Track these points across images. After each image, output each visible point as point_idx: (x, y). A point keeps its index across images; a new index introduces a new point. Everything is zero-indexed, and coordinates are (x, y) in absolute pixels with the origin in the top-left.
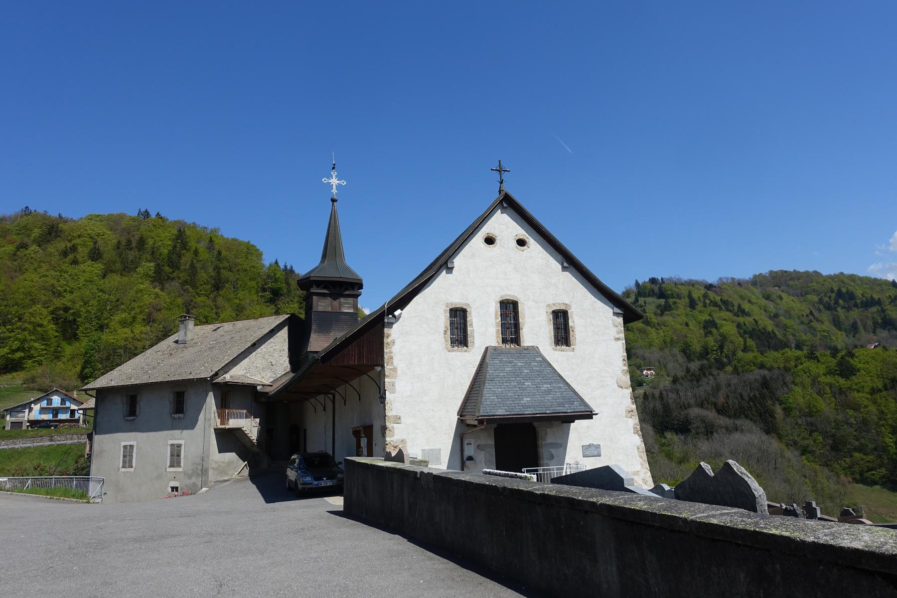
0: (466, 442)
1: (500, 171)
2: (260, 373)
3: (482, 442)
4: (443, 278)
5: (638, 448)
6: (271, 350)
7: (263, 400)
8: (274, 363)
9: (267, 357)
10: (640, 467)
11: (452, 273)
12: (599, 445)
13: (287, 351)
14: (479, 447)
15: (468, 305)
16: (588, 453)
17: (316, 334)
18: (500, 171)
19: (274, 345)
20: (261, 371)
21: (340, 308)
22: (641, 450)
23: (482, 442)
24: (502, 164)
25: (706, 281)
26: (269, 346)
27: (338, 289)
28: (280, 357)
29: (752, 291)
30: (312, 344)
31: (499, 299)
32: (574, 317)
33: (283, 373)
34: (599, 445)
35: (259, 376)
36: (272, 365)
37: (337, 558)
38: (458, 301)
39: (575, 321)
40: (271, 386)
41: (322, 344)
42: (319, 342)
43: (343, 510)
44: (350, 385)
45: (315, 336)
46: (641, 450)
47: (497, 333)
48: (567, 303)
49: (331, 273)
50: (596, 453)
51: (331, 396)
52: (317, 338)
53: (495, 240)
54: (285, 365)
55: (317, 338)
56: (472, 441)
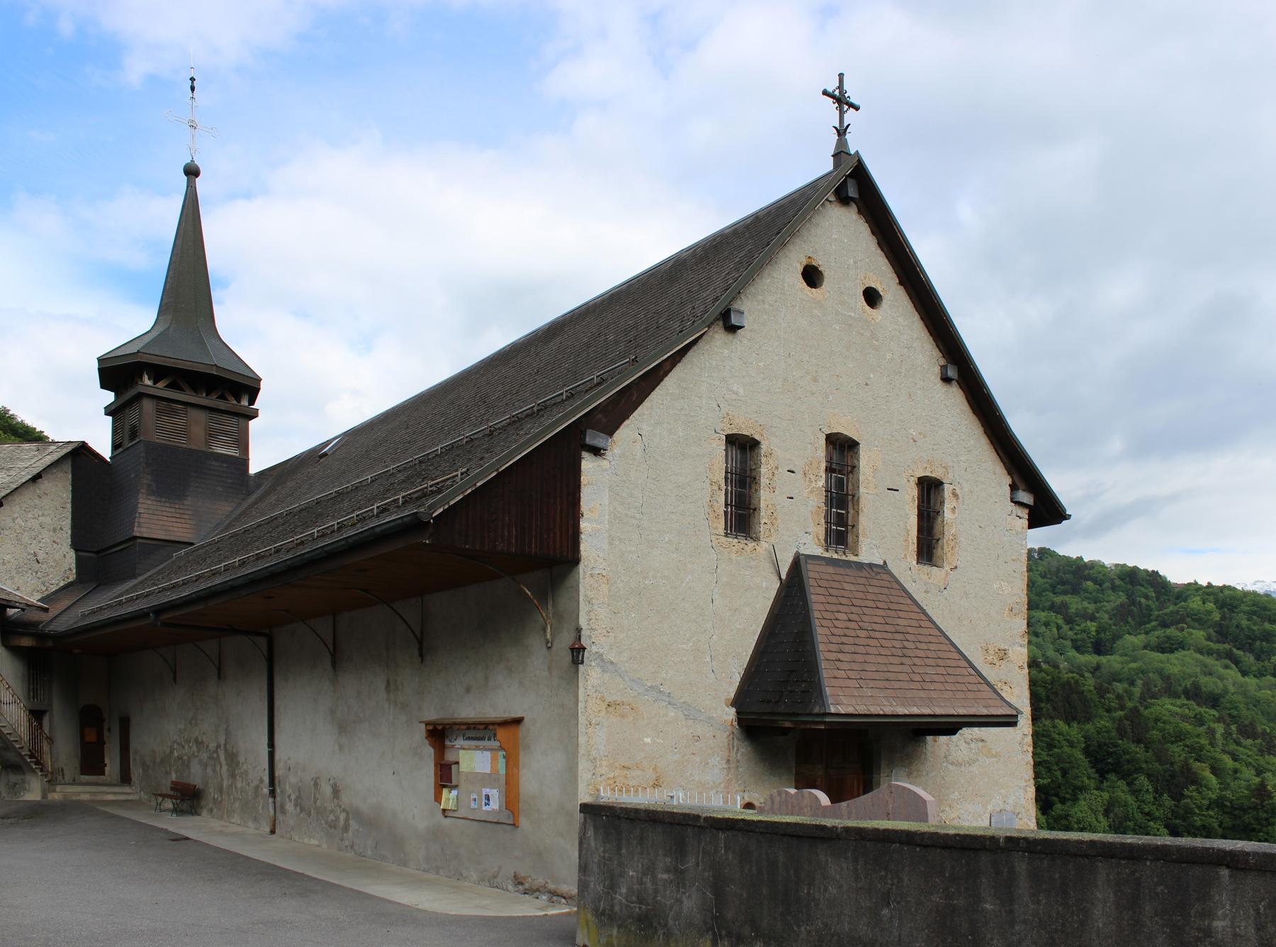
1: (841, 100)
2: (12, 578)
6: (35, 524)
7: (26, 642)
8: (41, 556)
9: (26, 538)
11: (100, 360)
13: (70, 532)
17: (153, 498)
18: (841, 100)
19: (40, 514)
20: (14, 573)
21: (207, 443)
26: (30, 515)
27: (204, 395)
28: (55, 545)
30: (142, 520)
33: (62, 584)
35: (9, 582)
36: (38, 562)
39: (952, 515)
40: (46, 610)
41: (166, 523)
42: (160, 518)
44: (393, 609)
45: (149, 502)
49: (186, 355)
51: (262, 642)
52: (154, 507)
54: (66, 566)
55: (154, 507)
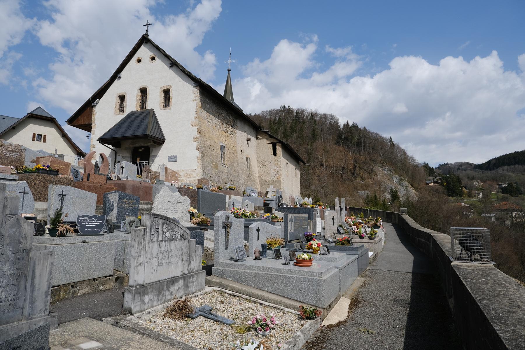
0: (118, 155)
3: (124, 155)
4: (116, 81)
5: (198, 158)
10: (197, 167)
12: (176, 156)
14: (123, 157)
15: (126, 93)
16: (170, 160)
22: (199, 159)
23: (124, 155)
24: (145, 24)
25: (155, 156)
29: (106, 203)
31: (139, 88)
32: (173, 91)
34: (176, 156)
37: (394, 316)
38: (121, 92)
39: (173, 95)
43: (96, 195)
46: (199, 159)
47: (137, 101)
48: (170, 85)
50: (174, 160)
53: (139, 59)
56: (120, 155)
